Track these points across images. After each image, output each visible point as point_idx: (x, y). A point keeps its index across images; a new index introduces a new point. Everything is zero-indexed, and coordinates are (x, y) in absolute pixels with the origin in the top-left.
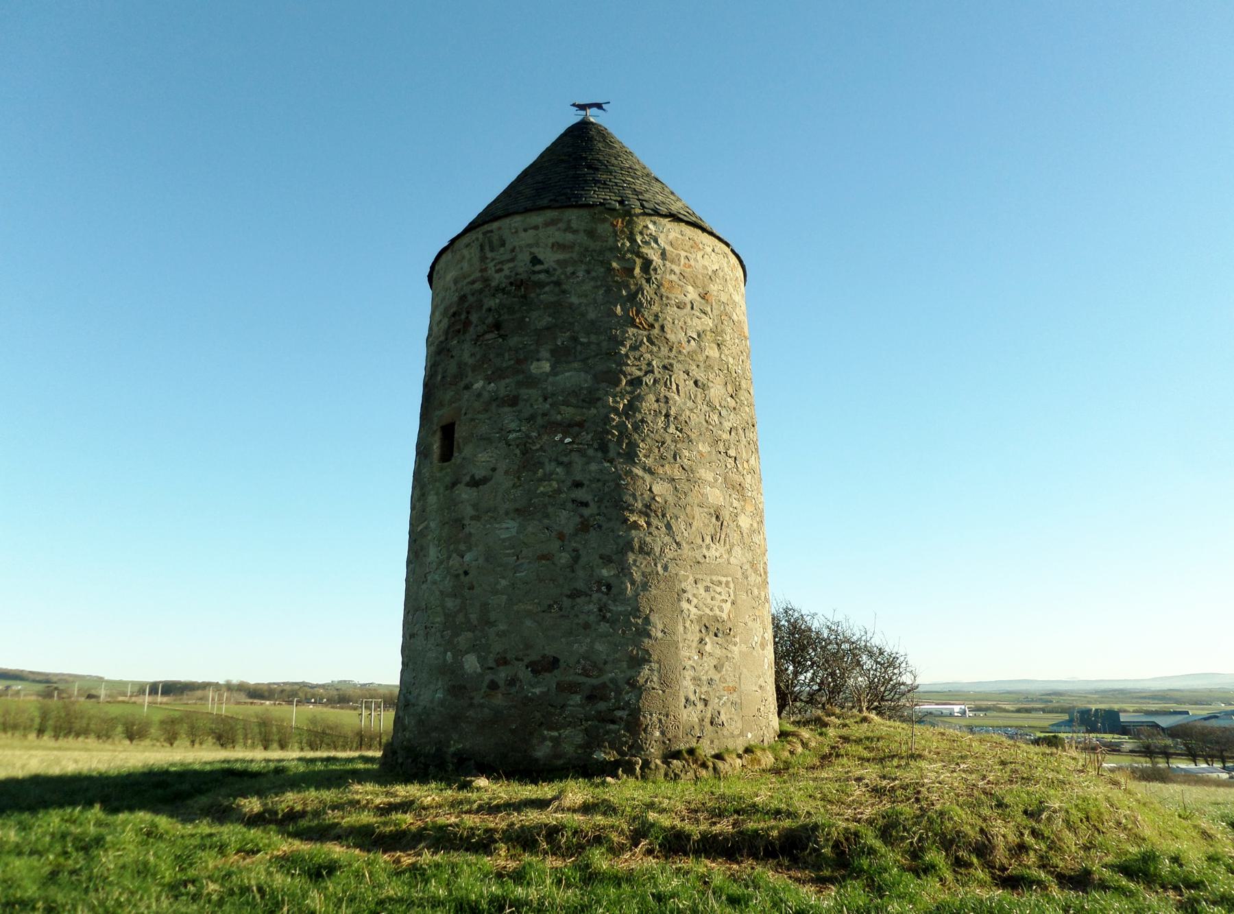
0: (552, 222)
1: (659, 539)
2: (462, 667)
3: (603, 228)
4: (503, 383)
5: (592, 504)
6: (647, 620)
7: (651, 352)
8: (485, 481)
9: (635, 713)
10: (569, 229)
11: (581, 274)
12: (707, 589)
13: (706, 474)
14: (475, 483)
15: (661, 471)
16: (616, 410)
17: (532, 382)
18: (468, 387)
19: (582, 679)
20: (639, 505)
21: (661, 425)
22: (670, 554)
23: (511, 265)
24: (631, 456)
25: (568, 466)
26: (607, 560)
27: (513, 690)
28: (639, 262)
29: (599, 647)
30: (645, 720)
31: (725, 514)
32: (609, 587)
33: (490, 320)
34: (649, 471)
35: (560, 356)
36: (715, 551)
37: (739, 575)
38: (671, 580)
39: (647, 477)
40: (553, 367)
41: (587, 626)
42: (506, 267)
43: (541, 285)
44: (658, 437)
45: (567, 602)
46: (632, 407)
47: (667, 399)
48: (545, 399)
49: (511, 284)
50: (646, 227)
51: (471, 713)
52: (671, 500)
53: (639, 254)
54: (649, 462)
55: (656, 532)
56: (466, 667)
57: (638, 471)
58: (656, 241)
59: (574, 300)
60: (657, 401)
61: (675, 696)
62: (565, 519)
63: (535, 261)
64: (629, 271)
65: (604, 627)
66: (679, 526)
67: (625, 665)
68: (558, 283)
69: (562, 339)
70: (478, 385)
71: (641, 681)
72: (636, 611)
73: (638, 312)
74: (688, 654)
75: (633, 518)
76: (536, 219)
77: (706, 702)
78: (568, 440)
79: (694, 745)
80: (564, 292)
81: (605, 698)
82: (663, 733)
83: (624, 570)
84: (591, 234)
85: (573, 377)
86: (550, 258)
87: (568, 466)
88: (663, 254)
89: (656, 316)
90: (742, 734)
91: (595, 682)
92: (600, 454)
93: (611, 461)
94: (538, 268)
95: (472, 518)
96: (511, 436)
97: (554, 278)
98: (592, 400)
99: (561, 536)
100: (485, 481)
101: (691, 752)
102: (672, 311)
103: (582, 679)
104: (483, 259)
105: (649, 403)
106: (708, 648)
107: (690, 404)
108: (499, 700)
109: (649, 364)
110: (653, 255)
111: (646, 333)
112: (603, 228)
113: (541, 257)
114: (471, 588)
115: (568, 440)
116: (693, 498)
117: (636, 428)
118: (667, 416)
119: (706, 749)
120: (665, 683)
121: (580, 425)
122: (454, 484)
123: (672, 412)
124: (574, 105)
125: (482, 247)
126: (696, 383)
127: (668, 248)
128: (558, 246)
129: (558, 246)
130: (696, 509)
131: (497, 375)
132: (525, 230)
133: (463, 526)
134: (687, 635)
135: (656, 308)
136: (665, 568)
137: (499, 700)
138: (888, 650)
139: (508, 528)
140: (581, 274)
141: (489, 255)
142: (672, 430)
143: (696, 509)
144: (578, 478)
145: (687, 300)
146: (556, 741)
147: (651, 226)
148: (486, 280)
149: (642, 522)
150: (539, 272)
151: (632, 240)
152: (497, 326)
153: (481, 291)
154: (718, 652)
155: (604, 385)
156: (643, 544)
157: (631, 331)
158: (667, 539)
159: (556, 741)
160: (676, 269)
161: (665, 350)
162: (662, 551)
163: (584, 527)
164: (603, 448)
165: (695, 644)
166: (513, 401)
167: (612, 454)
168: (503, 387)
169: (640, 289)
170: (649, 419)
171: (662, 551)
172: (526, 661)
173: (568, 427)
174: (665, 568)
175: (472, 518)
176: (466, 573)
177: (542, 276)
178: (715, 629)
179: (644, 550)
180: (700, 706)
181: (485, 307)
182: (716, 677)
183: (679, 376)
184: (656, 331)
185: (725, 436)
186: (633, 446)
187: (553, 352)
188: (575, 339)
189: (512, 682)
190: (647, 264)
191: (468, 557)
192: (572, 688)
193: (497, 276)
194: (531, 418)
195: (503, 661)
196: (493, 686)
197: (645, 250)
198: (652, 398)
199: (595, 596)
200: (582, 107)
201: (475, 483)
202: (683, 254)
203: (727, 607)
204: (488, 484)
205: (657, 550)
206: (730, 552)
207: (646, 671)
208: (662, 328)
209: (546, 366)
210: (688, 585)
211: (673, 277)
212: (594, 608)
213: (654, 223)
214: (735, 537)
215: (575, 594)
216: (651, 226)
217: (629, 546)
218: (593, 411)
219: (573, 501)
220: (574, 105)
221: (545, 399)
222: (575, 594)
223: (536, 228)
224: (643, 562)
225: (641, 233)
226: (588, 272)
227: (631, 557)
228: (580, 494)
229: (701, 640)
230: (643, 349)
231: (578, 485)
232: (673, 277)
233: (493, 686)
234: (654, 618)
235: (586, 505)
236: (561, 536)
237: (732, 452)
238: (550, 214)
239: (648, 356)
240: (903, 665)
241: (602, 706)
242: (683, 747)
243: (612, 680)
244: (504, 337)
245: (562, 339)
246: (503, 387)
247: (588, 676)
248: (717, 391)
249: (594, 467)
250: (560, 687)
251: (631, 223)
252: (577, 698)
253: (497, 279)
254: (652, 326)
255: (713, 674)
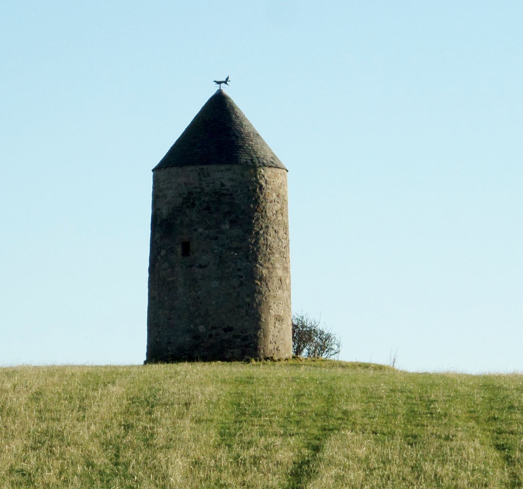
0: (229, 170)
1: (264, 289)
2: (198, 329)
3: (246, 173)
4: (211, 231)
5: (244, 277)
6: (260, 316)
7: (262, 222)
8: (205, 266)
9: (256, 345)
10: (234, 173)
11: (239, 192)
12: (277, 306)
13: (277, 265)
14: (201, 267)
15: (265, 265)
16: (251, 244)
17: (222, 232)
18: (196, 230)
19: (240, 334)
20: (258, 277)
21: (265, 249)
22: (267, 294)
23: (213, 185)
24: (256, 260)
25: (235, 263)
26: (248, 296)
27: (217, 337)
28: (258, 186)
29: (246, 324)
30: (259, 347)
31: (283, 279)
32: (249, 305)
33: (205, 205)
34: (261, 265)
35: (233, 223)
36: (280, 292)
37: (286, 301)
38: (267, 302)
39: (261, 267)
40: (230, 228)
41: (242, 317)
42: (211, 185)
43: (224, 195)
44: (264, 253)
45: (236, 309)
46: (256, 242)
47: (267, 239)
48: (227, 239)
49: (213, 193)
50: (261, 171)
51: (203, 344)
52: (268, 275)
53: (258, 183)
54: (261, 262)
55: (263, 286)
56: (200, 329)
57: (258, 265)
58: (264, 177)
59: (237, 201)
60: (264, 240)
61: (268, 341)
62: (235, 282)
63: (223, 185)
64: (255, 190)
65: (247, 318)
66: (270, 284)
67: (253, 330)
68: (231, 195)
69: (233, 217)
70: (201, 230)
71: (258, 335)
72: (257, 313)
73: (258, 206)
74: (271, 327)
75: (257, 282)
76: (222, 167)
77: (275, 343)
78: (236, 254)
79: (272, 356)
80: (233, 198)
81: (248, 340)
82: (264, 352)
83: (254, 299)
84: (242, 175)
85: (237, 231)
86: (228, 184)
87: (235, 263)
88: (266, 182)
89: (264, 207)
90: (285, 354)
91: (245, 335)
92: (246, 260)
93: (249, 262)
94: (224, 188)
95: (201, 279)
96: (215, 251)
97: (229, 193)
98: (244, 240)
99: (234, 288)
100: (205, 266)
101: (272, 358)
102: (269, 204)
103: (240, 334)
104: (200, 180)
105: (262, 241)
106: (277, 325)
107: (273, 240)
108: (212, 340)
109: (262, 226)
110: (264, 184)
111: (260, 214)
112: (246, 173)
113: (225, 183)
114: (201, 303)
115: (236, 254)
116: (274, 274)
117: (258, 250)
118: (267, 245)
119: (276, 358)
120: (265, 336)
121: (240, 248)
122: (191, 266)
123: (269, 244)
124: (215, 81)
125: (199, 175)
126: (275, 231)
127: (268, 179)
128: (231, 180)
129: (231, 180)
130: (275, 278)
131: (208, 228)
132: (218, 172)
133: (197, 282)
134: (271, 321)
135: (264, 204)
136: (266, 298)
137: (212, 340)
138: (326, 332)
139: (215, 284)
140: (239, 192)
141: (203, 179)
142: (268, 250)
143: (275, 278)
144: (239, 267)
145: (273, 199)
146: (233, 353)
147: (262, 171)
148: (202, 189)
149: (259, 283)
150: (224, 190)
151: (256, 177)
152: (208, 208)
153: (200, 193)
154: (279, 327)
155: (247, 234)
156: (259, 290)
157: (256, 214)
158: (266, 289)
159: (233, 353)
160: (270, 187)
161: (266, 220)
162: (265, 293)
163: (241, 284)
164: (247, 257)
165: (273, 324)
166: (216, 238)
167: (250, 259)
168: (212, 232)
169: (259, 197)
170: (261, 246)
171: (265, 293)
172: (223, 328)
173: (237, 249)
174: (266, 298)
175: (201, 279)
176: (198, 298)
177: (225, 192)
178: (279, 319)
179: (260, 293)
180: (274, 344)
181: (202, 200)
182: (278, 335)
183: (271, 230)
184: (264, 213)
185: (283, 250)
186: (257, 257)
187: (230, 222)
188: (237, 217)
189: (217, 334)
190: (261, 186)
191: (199, 293)
192: (238, 337)
193: (207, 188)
194: (223, 246)
195: (214, 328)
196: (211, 336)
197: (260, 181)
198: (262, 238)
199: (245, 307)
200: (219, 83)
201: (201, 267)
202: (272, 180)
203: (282, 311)
204: (207, 268)
205: (263, 293)
206: (283, 293)
207: (259, 332)
208: (266, 212)
209: (227, 227)
210: (272, 304)
211: (269, 191)
212: (244, 311)
213: (263, 169)
214: (285, 288)
215: (238, 307)
216: (262, 171)
217: (255, 291)
218: (244, 244)
219: (238, 275)
220: (215, 81)
221: (227, 239)
222: (238, 307)
223: (222, 171)
224: (259, 297)
225: (259, 174)
226: (241, 191)
227: (256, 295)
228: (240, 273)
229: (275, 323)
230: (260, 221)
231: (239, 270)
232: (269, 191)
233: (211, 336)
234: (263, 315)
235: (241, 277)
236: (234, 288)
237: (285, 256)
238: (227, 166)
239: (261, 223)
240: (333, 340)
241: (247, 342)
242: (269, 356)
243: (250, 335)
244: (211, 213)
245: (233, 217)
246: (212, 232)
247: (242, 333)
248: (281, 233)
249: (244, 264)
250: (234, 336)
251: (256, 171)
252: (239, 340)
253: (207, 190)
254: (262, 211)
255: (277, 334)
